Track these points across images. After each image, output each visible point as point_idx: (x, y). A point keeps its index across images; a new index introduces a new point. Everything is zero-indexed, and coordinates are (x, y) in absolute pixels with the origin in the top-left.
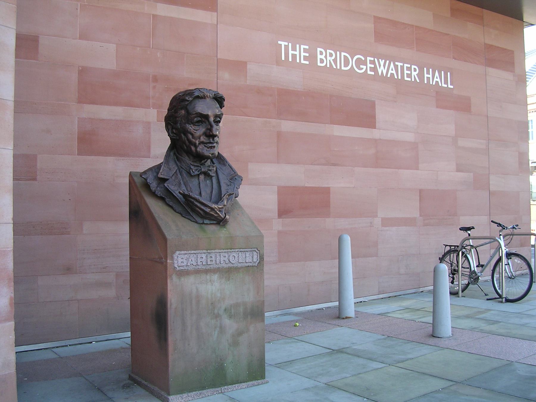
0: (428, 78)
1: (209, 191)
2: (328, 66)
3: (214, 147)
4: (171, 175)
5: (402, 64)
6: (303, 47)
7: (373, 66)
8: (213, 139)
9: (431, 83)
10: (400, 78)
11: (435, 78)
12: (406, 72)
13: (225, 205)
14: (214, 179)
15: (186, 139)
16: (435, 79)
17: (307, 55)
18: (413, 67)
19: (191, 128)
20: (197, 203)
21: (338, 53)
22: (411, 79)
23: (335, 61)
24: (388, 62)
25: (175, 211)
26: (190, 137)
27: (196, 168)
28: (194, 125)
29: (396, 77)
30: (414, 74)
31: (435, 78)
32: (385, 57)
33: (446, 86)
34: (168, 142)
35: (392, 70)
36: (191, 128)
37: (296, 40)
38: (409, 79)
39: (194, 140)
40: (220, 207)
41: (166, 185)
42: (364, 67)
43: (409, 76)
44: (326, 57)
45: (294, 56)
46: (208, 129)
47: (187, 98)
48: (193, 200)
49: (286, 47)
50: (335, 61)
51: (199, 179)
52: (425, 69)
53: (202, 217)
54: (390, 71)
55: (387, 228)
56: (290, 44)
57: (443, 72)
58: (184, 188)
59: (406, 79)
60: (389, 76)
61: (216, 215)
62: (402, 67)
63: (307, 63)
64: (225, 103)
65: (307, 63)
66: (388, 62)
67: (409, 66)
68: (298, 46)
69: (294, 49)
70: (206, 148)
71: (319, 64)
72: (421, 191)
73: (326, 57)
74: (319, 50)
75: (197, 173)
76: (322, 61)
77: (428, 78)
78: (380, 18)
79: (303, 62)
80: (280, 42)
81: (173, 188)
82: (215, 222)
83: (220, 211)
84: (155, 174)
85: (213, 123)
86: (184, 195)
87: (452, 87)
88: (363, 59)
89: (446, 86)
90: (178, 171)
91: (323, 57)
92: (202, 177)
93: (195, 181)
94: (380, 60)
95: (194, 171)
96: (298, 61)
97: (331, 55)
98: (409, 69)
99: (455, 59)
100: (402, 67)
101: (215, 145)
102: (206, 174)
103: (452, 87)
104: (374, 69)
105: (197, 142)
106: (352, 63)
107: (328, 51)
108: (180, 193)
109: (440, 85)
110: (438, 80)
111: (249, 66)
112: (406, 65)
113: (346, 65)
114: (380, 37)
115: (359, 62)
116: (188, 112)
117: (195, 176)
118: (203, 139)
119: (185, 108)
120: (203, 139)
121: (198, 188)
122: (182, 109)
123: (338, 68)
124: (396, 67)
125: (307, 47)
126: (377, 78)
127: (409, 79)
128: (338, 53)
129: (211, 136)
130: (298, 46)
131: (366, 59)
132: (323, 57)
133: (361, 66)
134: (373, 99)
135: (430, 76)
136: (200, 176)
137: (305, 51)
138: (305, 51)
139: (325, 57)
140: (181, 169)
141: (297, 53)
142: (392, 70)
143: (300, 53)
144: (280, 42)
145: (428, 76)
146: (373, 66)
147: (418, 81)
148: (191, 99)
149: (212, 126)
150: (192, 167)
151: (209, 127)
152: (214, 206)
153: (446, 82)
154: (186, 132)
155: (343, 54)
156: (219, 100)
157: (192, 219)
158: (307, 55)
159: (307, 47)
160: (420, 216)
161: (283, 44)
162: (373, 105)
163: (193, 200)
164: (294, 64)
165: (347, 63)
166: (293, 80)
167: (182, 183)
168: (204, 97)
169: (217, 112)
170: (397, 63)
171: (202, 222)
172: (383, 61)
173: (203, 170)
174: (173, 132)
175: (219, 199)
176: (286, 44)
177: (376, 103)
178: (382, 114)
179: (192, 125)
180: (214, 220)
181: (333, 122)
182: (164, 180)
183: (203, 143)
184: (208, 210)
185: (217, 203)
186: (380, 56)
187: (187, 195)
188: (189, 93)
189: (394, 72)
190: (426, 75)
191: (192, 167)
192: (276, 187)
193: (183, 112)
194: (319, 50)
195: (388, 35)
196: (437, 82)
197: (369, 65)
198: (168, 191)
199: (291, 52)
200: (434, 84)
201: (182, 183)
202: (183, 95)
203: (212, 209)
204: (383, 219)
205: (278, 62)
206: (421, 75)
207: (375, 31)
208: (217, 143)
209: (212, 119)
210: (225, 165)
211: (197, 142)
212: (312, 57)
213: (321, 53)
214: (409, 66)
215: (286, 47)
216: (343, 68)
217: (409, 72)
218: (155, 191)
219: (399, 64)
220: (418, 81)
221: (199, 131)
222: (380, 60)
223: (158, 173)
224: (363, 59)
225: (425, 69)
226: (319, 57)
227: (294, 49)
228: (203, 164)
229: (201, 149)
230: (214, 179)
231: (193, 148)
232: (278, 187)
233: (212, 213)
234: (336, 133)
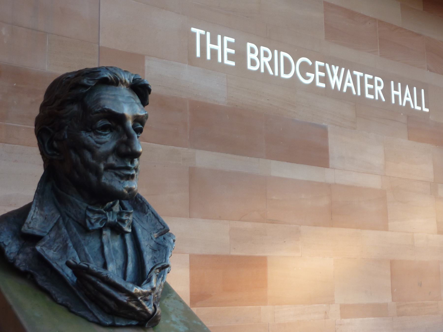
0: (396, 97)
1: (120, 262)
2: (262, 70)
3: (132, 176)
4: (48, 231)
5: (361, 74)
6: (226, 39)
7: (323, 74)
8: (132, 162)
9: (401, 104)
10: (359, 94)
11: (406, 97)
12: (367, 86)
13: (153, 289)
14: (128, 237)
15: (79, 159)
16: (406, 99)
17: (233, 51)
18: (377, 79)
19: (89, 138)
20: (103, 285)
21: (276, 52)
22: (375, 97)
23: (272, 63)
24: (343, 70)
25: (55, 300)
26: (88, 156)
27: (96, 216)
28: (97, 134)
29: (354, 93)
30: (379, 89)
31: (406, 97)
32: (340, 63)
33: (419, 108)
34: (37, 168)
35: (349, 82)
36: (89, 138)
37: (216, 28)
38: (372, 97)
39: (94, 162)
40: (145, 291)
41: (38, 248)
42: (312, 75)
43: (372, 92)
44: (259, 57)
45: (214, 53)
46: (121, 143)
47: (85, 81)
48: (93, 279)
49: (203, 38)
50: (272, 63)
51: (101, 238)
52: (392, 83)
53: (111, 313)
54: (347, 84)
55: (348, 320)
56: (208, 34)
57: (415, 88)
58: (75, 254)
59: (368, 96)
60: (345, 90)
61: (138, 309)
62: (362, 79)
63: (233, 63)
64: (151, 97)
65: (233, 63)
66: (343, 70)
67: (371, 77)
68: (219, 37)
69: (214, 41)
70: (117, 178)
71: (250, 67)
72: (392, 263)
73: (259, 57)
74: (249, 45)
75: (98, 225)
76: (253, 63)
77: (396, 97)
78: (332, 6)
79: (227, 62)
80: (193, 29)
81: (51, 254)
82: (134, 323)
83: (146, 300)
84: (15, 227)
85: (133, 131)
86: (77, 270)
87: (427, 110)
88: (310, 63)
89: (419, 108)
90: (61, 222)
91: (254, 56)
92: (107, 233)
93: (94, 243)
94: (333, 66)
95: (94, 221)
96: (220, 60)
97: (266, 55)
98: (371, 82)
99: (431, 71)
100: (362, 79)
101: (134, 172)
102: (117, 230)
103: (427, 110)
104: (325, 80)
105: (102, 167)
106: (295, 68)
107: (263, 48)
108: (68, 264)
109: (412, 107)
110: (410, 99)
111: (147, 63)
112: (367, 76)
113: (303, 64)
114: (332, 33)
115: (304, 68)
116: (85, 108)
117: (94, 230)
118: (112, 160)
119: (80, 100)
120: (112, 160)
121: (100, 257)
122: (73, 101)
123: (276, 74)
124: (354, 78)
125: (232, 40)
126: (330, 93)
127: (372, 97)
128: (276, 52)
129: (127, 154)
130: (219, 37)
131: (314, 64)
132: (254, 56)
133: (308, 74)
134: (324, 124)
135: (399, 93)
136: (104, 232)
137: (230, 45)
138: (230, 45)
139: (260, 58)
140: (67, 219)
141: (218, 48)
142: (349, 82)
143: (222, 48)
144: (193, 29)
145: (396, 93)
146: (323, 74)
147: (384, 100)
148: (92, 83)
149: (130, 137)
150: (90, 215)
151: (125, 138)
152: (137, 290)
153: (419, 104)
154: (81, 147)
155: (283, 54)
156: (141, 90)
157: (89, 316)
158: (233, 51)
159: (232, 40)
160: (393, 300)
161: (198, 32)
162: (323, 132)
163: (93, 279)
164: (213, 65)
165: (287, 70)
166: (214, 90)
167: (70, 244)
168: (115, 82)
169: (140, 111)
170: (355, 72)
171: (109, 323)
172: (337, 67)
173: (110, 219)
174: (52, 147)
175: (141, 277)
176: (203, 32)
177: (329, 129)
178: (336, 146)
179: (92, 134)
180: (133, 319)
181: (272, 156)
182: (35, 239)
183: (110, 168)
184: (124, 299)
185: (139, 284)
186: (332, 61)
187: (84, 268)
188: (91, 73)
189: (351, 85)
190: (394, 92)
191: (90, 215)
192: (188, 255)
193: (75, 108)
194: (249, 45)
195: (342, 32)
196: (408, 103)
197: (319, 74)
198: (41, 260)
199: (209, 46)
200: (404, 104)
201: (70, 244)
202: (76, 76)
203: (133, 296)
204: (343, 307)
205: (191, 59)
206: (387, 91)
207: (325, 24)
208: (136, 169)
209: (130, 123)
210: (145, 213)
211: (102, 167)
212: (240, 56)
213: (252, 51)
214: (371, 77)
215: (203, 38)
216: (283, 76)
217: (371, 86)
218: (14, 260)
219: (358, 74)
220: (384, 100)
221: (108, 142)
222: (333, 66)
223: (21, 225)
224: (310, 63)
225: (392, 83)
226: (250, 56)
227: (214, 41)
228: (110, 209)
229: (108, 179)
230: (128, 237)
231: (93, 178)
232: (191, 256)
233: (132, 304)
234: (275, 173)
